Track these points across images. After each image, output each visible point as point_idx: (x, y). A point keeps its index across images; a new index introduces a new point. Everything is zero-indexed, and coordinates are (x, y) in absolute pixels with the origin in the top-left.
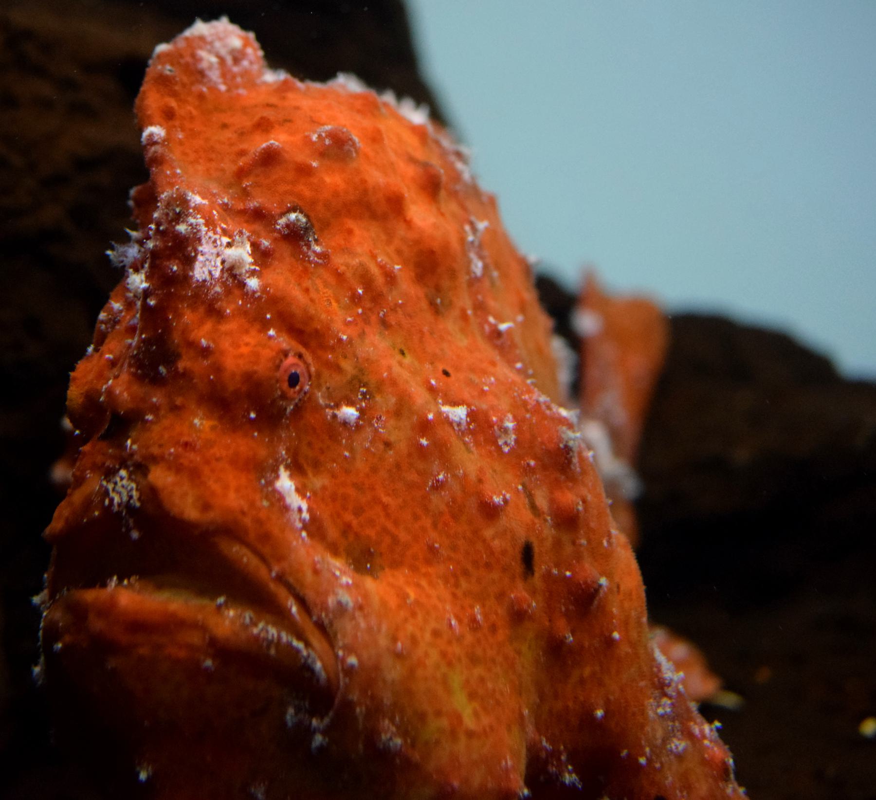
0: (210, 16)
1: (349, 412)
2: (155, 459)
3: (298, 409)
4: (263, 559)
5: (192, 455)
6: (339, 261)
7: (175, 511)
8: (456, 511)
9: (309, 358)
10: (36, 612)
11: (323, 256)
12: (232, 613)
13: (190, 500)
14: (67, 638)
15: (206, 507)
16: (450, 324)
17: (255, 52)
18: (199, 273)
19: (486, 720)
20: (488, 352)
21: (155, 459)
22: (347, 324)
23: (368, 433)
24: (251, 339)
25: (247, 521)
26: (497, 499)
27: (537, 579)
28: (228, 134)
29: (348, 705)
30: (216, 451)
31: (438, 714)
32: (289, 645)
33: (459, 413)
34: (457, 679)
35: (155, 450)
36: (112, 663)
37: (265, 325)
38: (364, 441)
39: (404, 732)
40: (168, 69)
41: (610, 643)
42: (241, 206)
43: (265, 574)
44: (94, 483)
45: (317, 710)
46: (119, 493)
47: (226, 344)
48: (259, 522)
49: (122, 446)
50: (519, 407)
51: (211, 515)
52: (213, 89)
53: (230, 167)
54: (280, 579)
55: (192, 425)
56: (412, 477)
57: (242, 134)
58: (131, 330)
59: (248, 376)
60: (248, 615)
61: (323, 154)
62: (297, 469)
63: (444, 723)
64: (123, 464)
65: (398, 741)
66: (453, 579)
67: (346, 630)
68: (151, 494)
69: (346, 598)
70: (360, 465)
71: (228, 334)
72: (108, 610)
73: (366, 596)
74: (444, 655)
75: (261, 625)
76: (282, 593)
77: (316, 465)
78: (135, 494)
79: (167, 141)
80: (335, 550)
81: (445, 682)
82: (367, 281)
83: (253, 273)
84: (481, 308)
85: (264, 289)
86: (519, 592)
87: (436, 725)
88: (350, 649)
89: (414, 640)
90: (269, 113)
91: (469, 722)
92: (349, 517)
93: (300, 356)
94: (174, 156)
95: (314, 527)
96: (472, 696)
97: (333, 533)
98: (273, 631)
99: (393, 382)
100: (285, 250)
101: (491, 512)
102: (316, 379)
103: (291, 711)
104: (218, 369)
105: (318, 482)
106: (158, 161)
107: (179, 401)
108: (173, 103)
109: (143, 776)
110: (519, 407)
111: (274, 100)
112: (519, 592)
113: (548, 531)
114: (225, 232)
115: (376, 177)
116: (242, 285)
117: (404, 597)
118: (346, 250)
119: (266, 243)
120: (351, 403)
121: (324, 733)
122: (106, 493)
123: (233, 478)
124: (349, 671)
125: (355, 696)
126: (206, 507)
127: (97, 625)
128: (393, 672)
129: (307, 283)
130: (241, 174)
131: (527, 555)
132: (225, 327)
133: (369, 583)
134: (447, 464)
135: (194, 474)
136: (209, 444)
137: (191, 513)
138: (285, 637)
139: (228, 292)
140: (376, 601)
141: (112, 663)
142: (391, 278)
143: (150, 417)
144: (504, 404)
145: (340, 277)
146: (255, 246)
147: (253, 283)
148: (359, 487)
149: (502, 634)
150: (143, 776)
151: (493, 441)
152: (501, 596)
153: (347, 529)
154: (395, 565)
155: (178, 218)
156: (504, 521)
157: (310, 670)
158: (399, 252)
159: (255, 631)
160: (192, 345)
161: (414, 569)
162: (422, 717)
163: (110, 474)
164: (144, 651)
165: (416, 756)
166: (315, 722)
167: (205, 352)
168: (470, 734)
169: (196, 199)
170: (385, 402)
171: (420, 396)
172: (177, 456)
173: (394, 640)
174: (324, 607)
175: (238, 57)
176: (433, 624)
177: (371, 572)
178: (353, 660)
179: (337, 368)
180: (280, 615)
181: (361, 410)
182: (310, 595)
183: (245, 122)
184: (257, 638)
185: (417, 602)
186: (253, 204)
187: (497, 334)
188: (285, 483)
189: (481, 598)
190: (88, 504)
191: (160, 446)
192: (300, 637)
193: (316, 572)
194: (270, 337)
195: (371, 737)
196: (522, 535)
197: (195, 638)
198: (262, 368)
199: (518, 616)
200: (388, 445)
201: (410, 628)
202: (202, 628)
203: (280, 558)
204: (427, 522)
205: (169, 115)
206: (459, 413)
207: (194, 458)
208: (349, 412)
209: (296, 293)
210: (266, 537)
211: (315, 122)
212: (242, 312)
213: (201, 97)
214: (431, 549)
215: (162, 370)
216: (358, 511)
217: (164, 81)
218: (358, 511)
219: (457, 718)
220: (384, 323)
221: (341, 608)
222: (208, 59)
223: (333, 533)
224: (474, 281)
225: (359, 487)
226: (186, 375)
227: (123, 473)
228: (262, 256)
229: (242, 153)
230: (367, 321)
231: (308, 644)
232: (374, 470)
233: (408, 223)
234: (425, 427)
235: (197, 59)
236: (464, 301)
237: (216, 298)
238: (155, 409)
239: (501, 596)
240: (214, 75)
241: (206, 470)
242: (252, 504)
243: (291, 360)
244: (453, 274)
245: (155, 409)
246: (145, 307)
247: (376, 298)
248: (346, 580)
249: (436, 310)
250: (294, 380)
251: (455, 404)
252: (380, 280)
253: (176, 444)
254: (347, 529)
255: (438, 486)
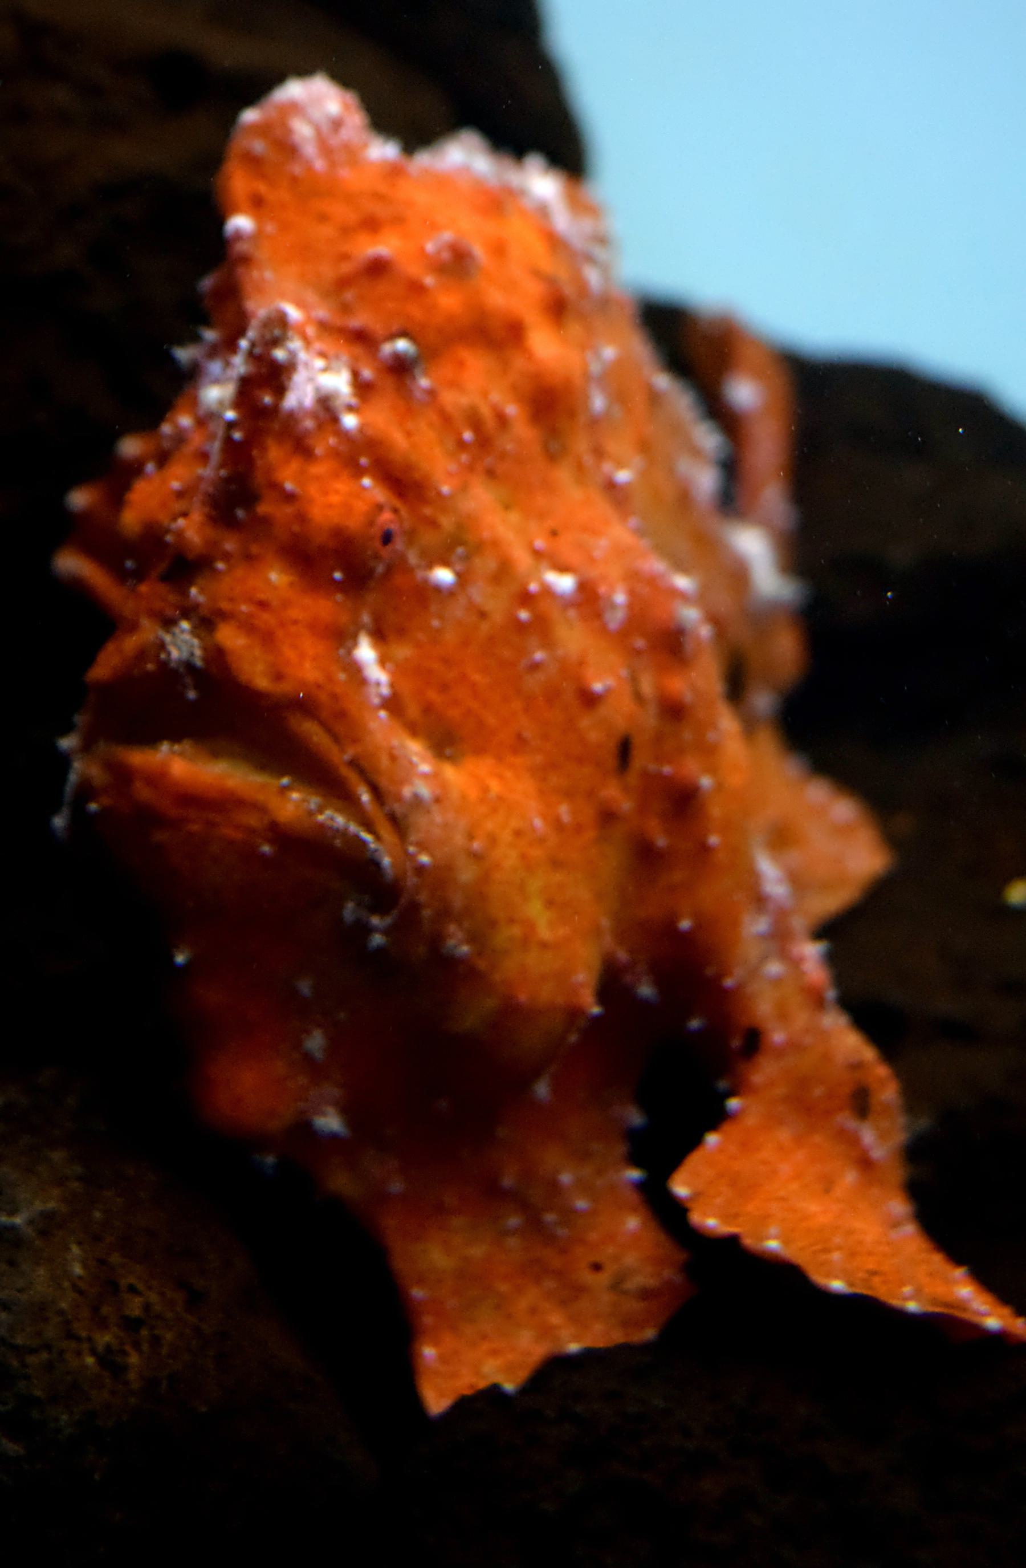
0: (304, 72)
1: (444, 575)
2: (224, 616)
3: (389, 570)
4: (336, 739)
5: (266, 616)
6: (450, 399)
7: (243, 678)
8: (552, 695)
9: (404, 512)
10: (64, 761)
11: (432, 393)
12: (295, 796)
13: (260, 667)
14: (106, 801)
15: (278, 677)
16: (563, 475)
17: (356, 120)
18: (291, 401)
19: (563, 931)
20: (602, 507)
21: (224, 616)
22: (450, 474)
23: (462, 600)
24: (341, 488)
25: (323, 697)
26: (598, 687)
27: (633, 778)
28: (327, 231)
29: (415, 907)
30: (294, 613)
31: (512, 921)
32: (357, 837)
33: (564, 583)
34: (535, 885)
35: (225, 605)
36: (160, 836)
37: (359, 472)
38: (457, 610)
39: (473, 938)
40: (258, 146)
41: (705, 849)
42: (339, 322)
43: (339, 757)
44: (149, 631)
45: (380, 907)
46: (179, 649)
47: (313, 490)
48: (335, 697)
49: (185, 594)
50: (634, 578)
51: (285, 688)
52: (309, 167)
53: (328, 271)
54: (354, 764)
55: (268, 581)
56: (506, 653)
57: (346, 231)
58: (203, 457)
59: (338, 532)
60: (314, 801)
61: (440, 268)
62: (379, 636)
63: (516, 931)
64: (186, 615)
65: (465, 949)
66: (541, 773)
67: (423, 825)
68: (217, 655)
69: (425, 791)
70: (451, 637)
71: (318, 478)
72: (157, 779)
73: (444, 785)
74: (523, 857)
75: (328, 813)
76: (351, 776)
77: (401, 632)
78: (198, 652)
79: (258, 236)
80: (413, 730)
81: (522, 888)
82: (475, 422)
83: (350, 408)
84: (599, 453)
85: (361, 429)
86: (612, 792)
87: (506, 934)
88: (423, 847)
89: (493, 840)
90: (380, 210)
91: (544, 932)
92: (433, 695)
93: (395, 511)
94: (262, 254)
95: (393, 704)
96: (550, 903)
97: (413, 711)
98: (340, 820)
99: (495, 543)
100: (389, 383)
101: (589, 700)
102: (411, 536)
103: (350, 906)
104: (302, 518)
105: (403, 651)
106: (246, 260)
107: (255, 549)
108: (262, 188)
109: (180, 959)
110: (634, 578)
111: (383, 188)
112: (612, 792)
113: (649, 719)
114: (323, 355)
115: (497, 299)
116: (335, 420)
117: (485, 790)
118: (454, 384)
119: (367, 373)
120: (446, 563)
121: (386, 932)
122: (162, 646)
123: (311, 646)
124: (420, 870)
125: (423, 897)
126: (278, 677)
127: (143, 792)
128: (467, 874)
129: (410, 425)
130: (343, 283)
131: (625, 750)
132: (317, 469)
133: (450, 772)
134: (548, 641)
135: (267, 639)
136: (286, 604)
137: (262, 683)
138: (353, 828)
139: (320, 426)
140: (455, 794)
141: (160, 836)
142: (502, 420)
143: (220, 565)
144: (615, 571)
145: (446, 419)
146: (355, 374)
147: (350, 421)
148: (446, 661)
149: (590, 834)
150: (180, 959)
151: (598, 615)
152: (591, 794)
153: (428, 709)
154: (479, 751)
155: (276, 342)
156: (603, 711)
157: (377, 864)
158: (514, 388)
159: (321, 818)
160: (276, 487)
161: (499, 758)
162: (493, 924)
163: (169, 623)
164: (195, 827)
165: (482, 965)
166: (375, 921)
167: (290, 498)
168: (544, 945)
169: (293, 313)
170: (487, 564)
171: (522, 559)
172: (250, 616)
173: (471, 837)
174: (399, 798)
175: (337, 124)
176: (515, 823)
177: (452, 759)
178: (425, 859)
179: (433, 524)
180: (346, 798)
181: (459, 575)
182: (384, 783)
183: (342, 212)
184: (321, 826)
185: (500, 798)
186: (356, 322)
187: (611, 486)
188: (366, 652)
189: (568, 794)
190: (142, 655)
191: (231, 600)
192: (370, 827)
193: (393, 758)
194: (364, 488)
195: (436, 940)
196: (621, 724)
197: (253, 820)
198: (354, 523)
199: (607, 817)
200: (483, 615)
201: (489, 825)
202: (260, 808)
203: (355, 741)
204: (517, 705)
205: (257, 205)
206: (564, 583)
207: (266, 619)
208: (444, 575)
209: (398, 439)
210: (342, 715)
211: (434, 227)
212: (334, 453)
213: (294, 180)
214: (519, 737)
215: (240, 513)
216: (444, 687)
217: (254, 162)
218: (444, 687)
219: (530, 927)
220: (491, 473)
221: (417, 801)
222: (302, 130)
223: (413, 711)
224: (595, 422)
225: (446, 661)
226: (266, 521)
227: (185, 625)
228: (362, 388)
229: (345, 257)
230: (471, 468)
231: (378, 838)
232: (465, 643)
233: (529, 355)
234: (526, 598)
235: (288, 131)
236: (581, 445)
237: (307, 433)
238: (226, 557)
239: (591, 794)
240: (310, 149)
241: (280, 633)
242: (330, 679)
243: (386, 516)
244: (572, 414)
245: (226, 557)
246: (228, 440)
247: (484, 442)
248: (425, 768)
249: (552, 457)
250: (387, 538)
251: (563, 568)
252: (490, 423)
253: (250, 600)
254: (428, 709)
255: (535, 667)
